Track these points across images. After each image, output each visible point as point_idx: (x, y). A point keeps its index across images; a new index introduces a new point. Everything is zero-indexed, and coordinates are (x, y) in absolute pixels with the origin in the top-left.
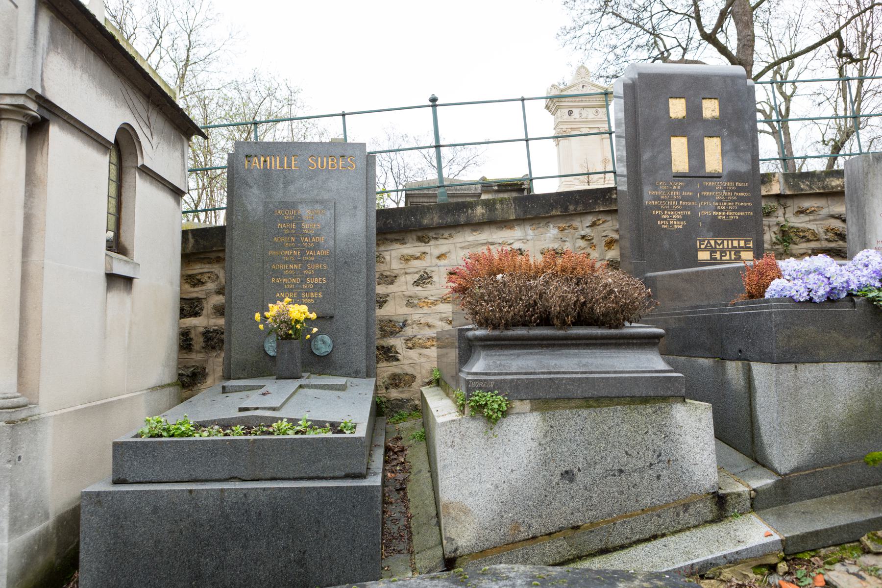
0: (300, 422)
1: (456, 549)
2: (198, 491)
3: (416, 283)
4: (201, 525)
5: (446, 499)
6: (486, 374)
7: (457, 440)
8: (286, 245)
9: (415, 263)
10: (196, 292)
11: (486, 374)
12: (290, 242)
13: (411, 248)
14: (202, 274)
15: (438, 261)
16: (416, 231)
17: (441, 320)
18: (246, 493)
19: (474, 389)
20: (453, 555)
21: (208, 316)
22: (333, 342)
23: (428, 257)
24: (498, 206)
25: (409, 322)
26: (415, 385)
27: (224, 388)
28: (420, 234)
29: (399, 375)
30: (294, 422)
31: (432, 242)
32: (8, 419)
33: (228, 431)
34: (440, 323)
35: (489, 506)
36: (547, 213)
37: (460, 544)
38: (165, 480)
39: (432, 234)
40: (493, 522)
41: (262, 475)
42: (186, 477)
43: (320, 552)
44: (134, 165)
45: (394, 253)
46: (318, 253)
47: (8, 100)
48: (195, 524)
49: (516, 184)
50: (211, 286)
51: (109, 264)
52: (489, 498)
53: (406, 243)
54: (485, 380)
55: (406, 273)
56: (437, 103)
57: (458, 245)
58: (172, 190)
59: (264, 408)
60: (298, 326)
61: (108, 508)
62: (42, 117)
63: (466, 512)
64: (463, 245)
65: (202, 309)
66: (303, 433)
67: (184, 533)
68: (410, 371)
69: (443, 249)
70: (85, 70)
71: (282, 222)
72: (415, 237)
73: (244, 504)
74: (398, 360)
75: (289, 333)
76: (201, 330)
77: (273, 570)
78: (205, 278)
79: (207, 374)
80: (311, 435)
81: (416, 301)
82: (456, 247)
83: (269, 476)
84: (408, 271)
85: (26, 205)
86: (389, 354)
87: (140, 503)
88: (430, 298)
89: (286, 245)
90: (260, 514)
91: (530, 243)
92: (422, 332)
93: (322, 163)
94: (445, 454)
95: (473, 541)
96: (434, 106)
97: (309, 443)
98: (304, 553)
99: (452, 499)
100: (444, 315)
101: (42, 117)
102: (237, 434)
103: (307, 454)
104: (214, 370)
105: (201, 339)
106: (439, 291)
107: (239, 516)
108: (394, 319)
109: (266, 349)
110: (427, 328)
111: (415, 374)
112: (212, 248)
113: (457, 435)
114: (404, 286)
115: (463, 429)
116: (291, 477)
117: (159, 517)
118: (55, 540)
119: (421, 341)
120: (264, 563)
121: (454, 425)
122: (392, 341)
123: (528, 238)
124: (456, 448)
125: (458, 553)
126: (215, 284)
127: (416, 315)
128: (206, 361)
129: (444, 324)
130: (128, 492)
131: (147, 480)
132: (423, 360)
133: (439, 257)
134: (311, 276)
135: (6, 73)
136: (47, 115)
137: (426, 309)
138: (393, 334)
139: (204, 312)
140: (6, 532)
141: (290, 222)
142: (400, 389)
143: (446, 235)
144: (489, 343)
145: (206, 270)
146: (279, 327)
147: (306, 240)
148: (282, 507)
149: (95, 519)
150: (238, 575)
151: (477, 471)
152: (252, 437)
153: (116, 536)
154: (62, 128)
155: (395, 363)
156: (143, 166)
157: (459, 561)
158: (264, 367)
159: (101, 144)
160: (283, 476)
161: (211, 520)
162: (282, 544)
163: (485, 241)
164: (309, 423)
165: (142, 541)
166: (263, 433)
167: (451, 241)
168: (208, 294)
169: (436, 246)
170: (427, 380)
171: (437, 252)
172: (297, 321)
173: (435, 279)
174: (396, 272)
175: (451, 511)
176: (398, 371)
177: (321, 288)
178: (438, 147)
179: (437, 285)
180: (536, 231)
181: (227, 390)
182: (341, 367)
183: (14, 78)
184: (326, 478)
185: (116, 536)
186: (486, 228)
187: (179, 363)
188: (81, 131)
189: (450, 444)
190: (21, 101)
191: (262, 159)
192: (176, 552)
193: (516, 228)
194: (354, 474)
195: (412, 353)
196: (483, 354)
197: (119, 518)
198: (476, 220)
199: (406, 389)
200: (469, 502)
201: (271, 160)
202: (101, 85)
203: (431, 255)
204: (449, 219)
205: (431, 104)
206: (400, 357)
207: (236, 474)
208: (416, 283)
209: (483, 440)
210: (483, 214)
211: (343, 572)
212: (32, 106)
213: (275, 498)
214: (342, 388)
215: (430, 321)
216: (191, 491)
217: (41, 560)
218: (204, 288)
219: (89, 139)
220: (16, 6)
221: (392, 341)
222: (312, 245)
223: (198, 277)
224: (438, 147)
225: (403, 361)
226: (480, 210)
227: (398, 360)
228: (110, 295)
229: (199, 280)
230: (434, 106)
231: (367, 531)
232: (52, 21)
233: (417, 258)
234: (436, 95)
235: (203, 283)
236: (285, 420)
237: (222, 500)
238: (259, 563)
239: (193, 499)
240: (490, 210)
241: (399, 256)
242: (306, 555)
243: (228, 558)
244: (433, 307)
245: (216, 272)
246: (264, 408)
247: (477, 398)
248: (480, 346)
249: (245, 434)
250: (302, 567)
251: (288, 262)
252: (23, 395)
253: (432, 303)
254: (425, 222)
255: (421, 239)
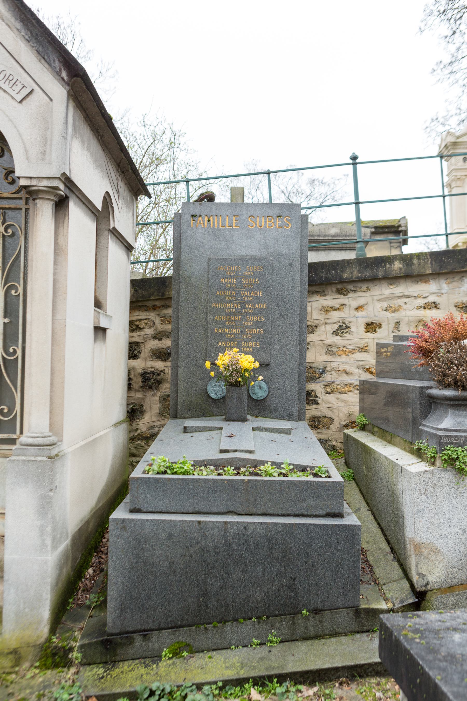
0: (282, 466)
1: (427, 584)
2: (206, 522)
3: (335, 333)
4: (208, 551)
5: (419, 539)
6: (456, 431)
7: (430, 489)
8: (228, 298)
9: (334, 314)
10: (137, 337)
11: (456, 431)
12: (231, 295)
13: (330, 300)
14: (140, 320)
15: (355, 312)
16: (336, 283)
17: (358, 367)
18: (246, 526)
19: (446, 444)
20: (424, 589)
21: (145, 359)
22: (269, 387)
23: (346, 309)
24: (415, 261)
25: (328, 369)
26: (334, 428)
27: (185, 428)
28: (339, 287)
29: (318, 418)
30: (278, 465)
31: (351, 295)
32: (48, 455)
33: (221, 471)
34: (357, 370)
35: (457, 548)
36: (463, 267)
37: (430, 579)
38: (173, 511)
39: (350, 287)
40: (460, 562)
41: (254, 510)
42: (191, 509)
43: (308, 580)
44: (107, 228)
45: (315, 305)
46: (257, 306)
47: (45, 183)
48: (203, 550)
49: (393, 227)
50: (148, 331)
51: (97, 319)
52: (457, 541)
53: (325, 295)
54: (456, 436)
55: (326, 323)
56: (358, 161)
57: (376, 298)
58: (126, 247)
59: (242, 451)
60: (247, 374)
61: (131, 532)
62: (66, 195)
63: (436, 552)
64: (380, 297)
65: (140, 352)
66: (285, 475)
67: (193, 557)
68: (328, 413)
69: (361, 301)
70: (89, 150)
71: (225, 277)
72: (334, 290)
73: (244, 535)
74: (317, 403)
75: (236, 381)
76: (140, 371)
77: (268, 592)
78: (143, 324)
79: (145, 411)
80: (293, 478)
81: (335, 350)
82: (373, 300)
83: (260, 511)
84: (328, 321)
85: (55, 274)
86: (310, 398)
87: (157, 530)
88: (348, 347)
89: (228, 298)
90: (257, 545)
91: (445, 296)
92: (341, 379)
93: (261, 222)
94: (419, 500)
95: (442, 578)
96: (355, 164)
97: (295, 485)
98: (294, 579)
99: (424, 540)
100: (361, 363)
101: (66, 195)
102: (229, 475)
103: (293, 494)
104: (151, 408)
105: (140, 380)
106: (356, 341)
107: (239, 545)
108: (314, 365)
109: (209, 392)
110: (345, 375)
111: (333, 417)
112: (150, 297)
113: (430, 484)
114: (323, 335)
115: (435, 479)
116: (280, 513)
117: (173, 542)
118: (71, 555)
119: (339, 387)
120: (260, 586)
121: (426, 475)
122: (312, 386)
123: (443, 291)
124: (429, 495)
125: (429, 587)
126: (152, 329)
127: (334, 362)
128: (144, 399)
129: (360, 371)
130: (147, 520)
131: (158, 510)
132: (340, 404)
133: (356, 309)
134: (250, 327)
135: (43, 159)
136: (69, 193)
137: (344, 358)
138: (313, 379)
139: (142, 355)
140: (49, 547)
141: (231, 277)
142: (319, 430)
143: (364, 288)
144: (457, 403)
145: (143, 317)
146: (231, 375)
147: (246, 294)
148: (276, 540)
149: (121, 542)
150: (238, 595)
151: (447, 516)
152: (242, 477)
153: (138, 556)
154: (75, 204)
155: (315, 406)
156: (114, 228)
157: (429, 594)
158: (209, 407)
159: (93, 212)
160: (272, 512)
161: (216, 547)
162: (276, 571)
163: (401, 294)
164: (291, 467)
165: (159, 562)
166: (252, 474)
167: (368, 293)
168: (146, 339)
169: (354, 298)
170: (344, 423)
171: (355, 304)
172: (246, 370)
173: (353, 329)
174: (317, 322)
175: (423, 550)
176: (317, 414)
177: (259, 338)
178: (357, 203)
179: (355, 335)
180: (450, 285)
181: (188, 430)
182: (275, 411)
183: (50, 163)
184: (309, 516)
185: (138, 556)
186: (402, 281)
187: (128, 399)
188: (84, 203)
189: (423, 491)
190: (56, 183)
191: (206, 219)
192: (187, 572)
193: (432, 282)
194: (334, 513)
195: (331, 398)
196: (450, 412)
197: (140, 542)
198: (394, 274)
199: (324, 430)
200: (439, 543)
201: (214, 219)
202: (96, 161)
203: (350, 306)
204: (368, 273)
205: (351, 161)
206: (319, 401)
207: (232, 509)
208: (335, 333)
209: (452, 490)
210: (400, 269)
211: (328, 597)
212: (62, 187)
213: (271, 532)
214: (288, 432)
215: (348, 368)
216: (199, 522)
217: (65, 571)
218: (142, 333)
219: (87, 209)
220: (51, 100)
221: (312, 386)
222: (251, 299)
223: (137, 323)
224: (357, 203)
225: (322, 405)
226: (397, 265)
227: (317, 403)
228: (96, 345)
229: (137, 326)
230: (355, 164)
231: (349, 564)
232: (74, 110)
233: (336, 310)
234: (357, 154)
235: (141, 329)
236: (270, 463)
237: (226, 530)
238: (256, 586)
239: (202, 529)
240: (407, 265)
241: (320, 307)
242: (296, 582)
243: (230, 580)
244: (351, 356)
245: (153, 318)
246: (242, 451)
247: (450, 452)
248: (448, 405)
249: (236, 475)
250: (292, 591)
251: (230, 314)
252: (54, 435)
253: (350, 352)
254: (345, 275)
255: (340, 292)
